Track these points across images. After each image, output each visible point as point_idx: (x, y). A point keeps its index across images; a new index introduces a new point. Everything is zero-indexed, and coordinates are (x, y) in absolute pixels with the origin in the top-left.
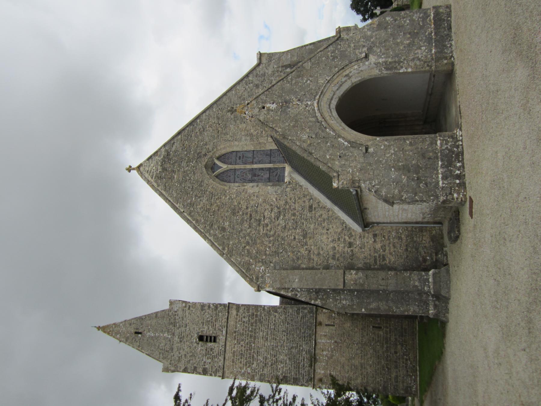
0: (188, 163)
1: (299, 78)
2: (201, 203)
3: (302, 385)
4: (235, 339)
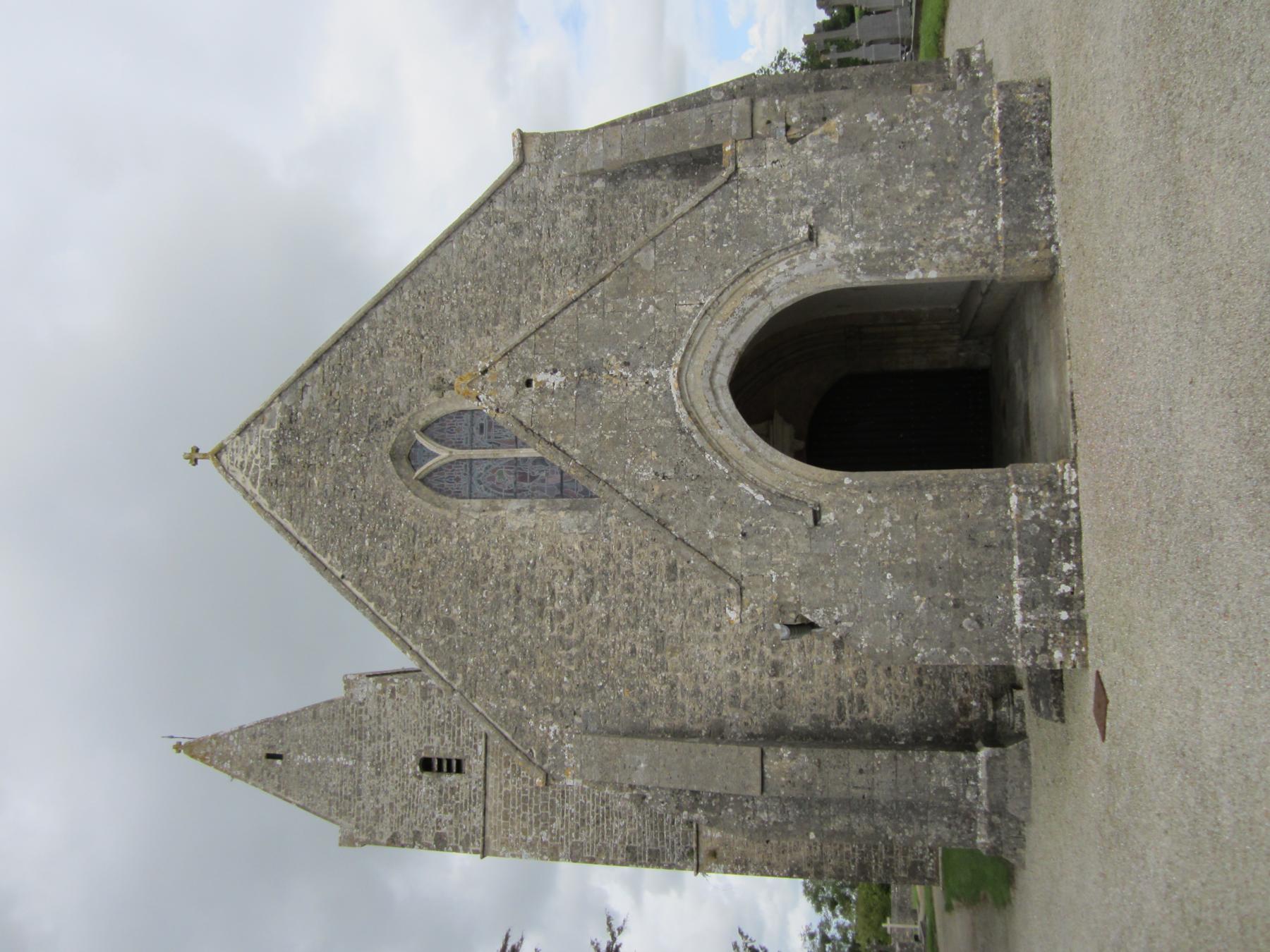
0: (347, 445)
1: (623, 296)
2: (388, 553)
3: (670, 867)
4: (507, 764)
